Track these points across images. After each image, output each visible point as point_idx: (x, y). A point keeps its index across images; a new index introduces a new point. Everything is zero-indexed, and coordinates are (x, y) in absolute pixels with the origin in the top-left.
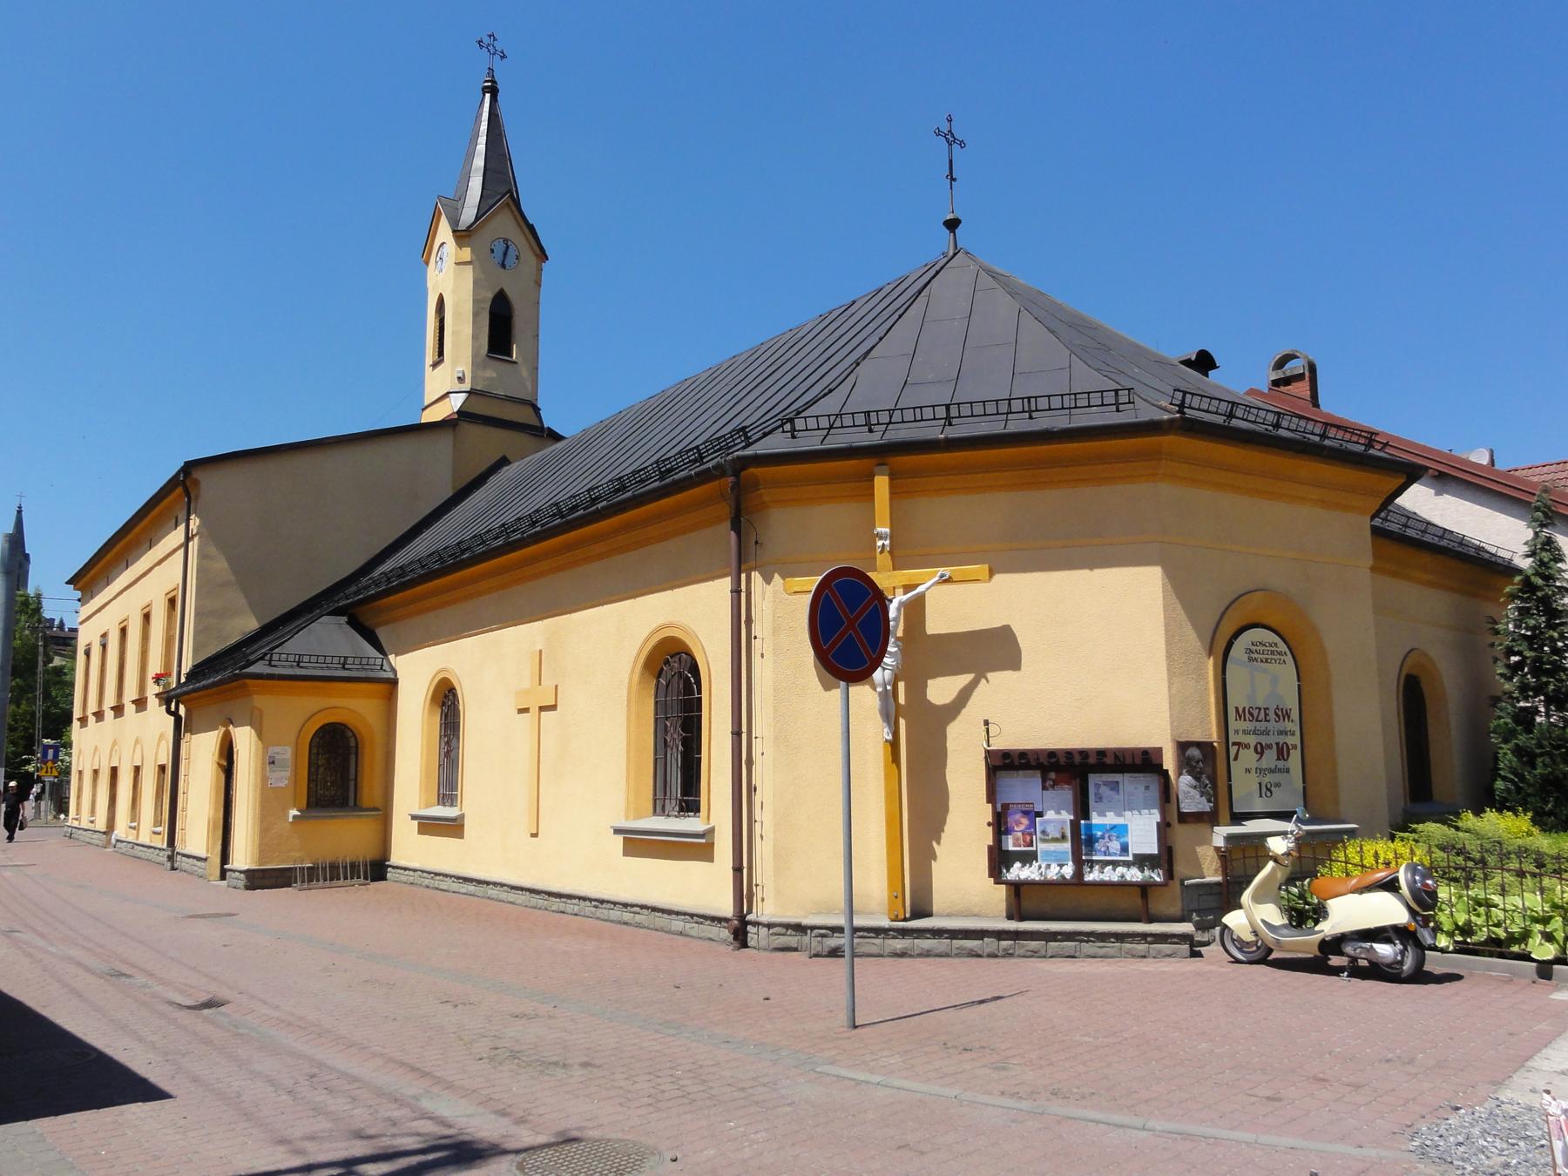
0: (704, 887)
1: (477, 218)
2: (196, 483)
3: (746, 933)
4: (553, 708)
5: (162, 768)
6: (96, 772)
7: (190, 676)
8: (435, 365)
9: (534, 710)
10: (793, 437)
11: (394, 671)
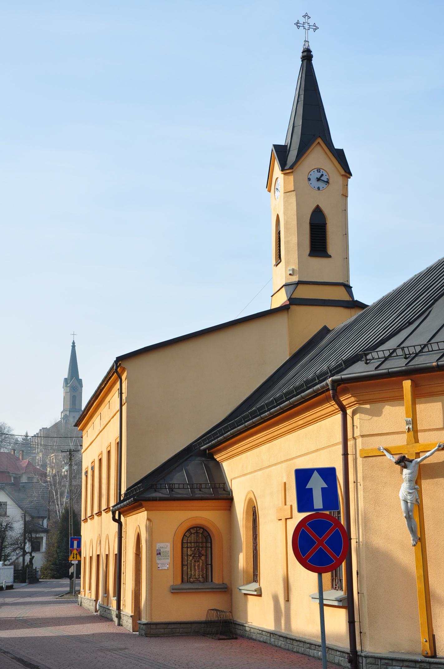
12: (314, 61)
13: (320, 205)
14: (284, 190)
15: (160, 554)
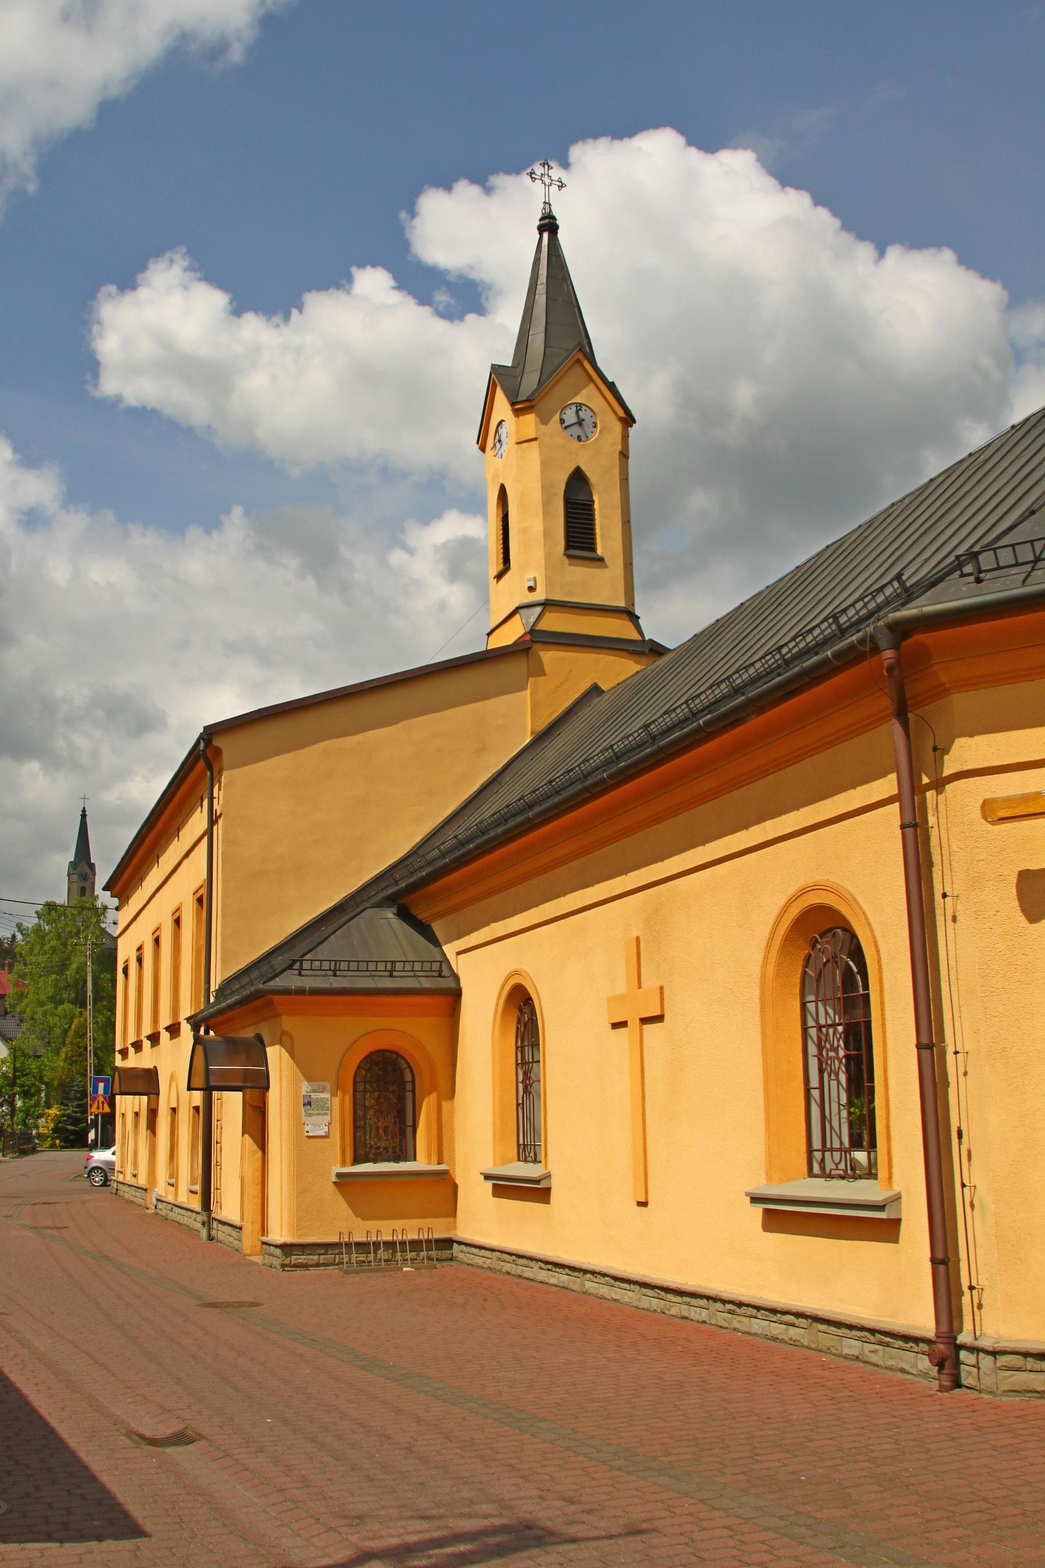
0: (882, 1286)
1: (540, 382)
2: (218, 752)
3: (957, 1363)
4: (659, 1018)
5: (197, 1108)
6: (137, 1114)
7: (221, 991)
8: (499, 576)
9: (634, 1024)
10: (978, 581)
11: (456, 978)
12: (561, 235)
13: (583, 468)
14: (518, 438)
15: (309, 1103)
